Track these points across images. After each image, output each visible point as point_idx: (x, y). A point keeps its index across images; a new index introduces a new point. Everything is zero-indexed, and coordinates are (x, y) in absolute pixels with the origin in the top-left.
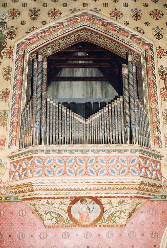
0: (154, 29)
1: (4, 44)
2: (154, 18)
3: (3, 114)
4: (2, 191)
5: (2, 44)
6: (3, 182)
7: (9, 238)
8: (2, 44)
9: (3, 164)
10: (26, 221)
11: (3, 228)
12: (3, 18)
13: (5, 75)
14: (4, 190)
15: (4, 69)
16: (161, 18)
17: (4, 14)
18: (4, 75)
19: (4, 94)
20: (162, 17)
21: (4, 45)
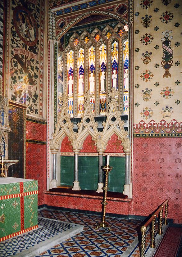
0: (143, 18)
1: (170, 62)
2: (143, 38)
3: (165, 109)
4: (136, 131)
5: (169, 62)
6: (146, 124)
7: (143, 166)
8: (169, 62)
9: (169, 109)
10: (142, 140)
11: (148, 155)
12: (167, 37)
13: (144, 60)
14: (147, 129)
15: (143, 18)
16: (143, 110)
17: (167, 33)
18: (143, 23)
19: (145, 76)
20: (142, 37)
21: (170, 64)
